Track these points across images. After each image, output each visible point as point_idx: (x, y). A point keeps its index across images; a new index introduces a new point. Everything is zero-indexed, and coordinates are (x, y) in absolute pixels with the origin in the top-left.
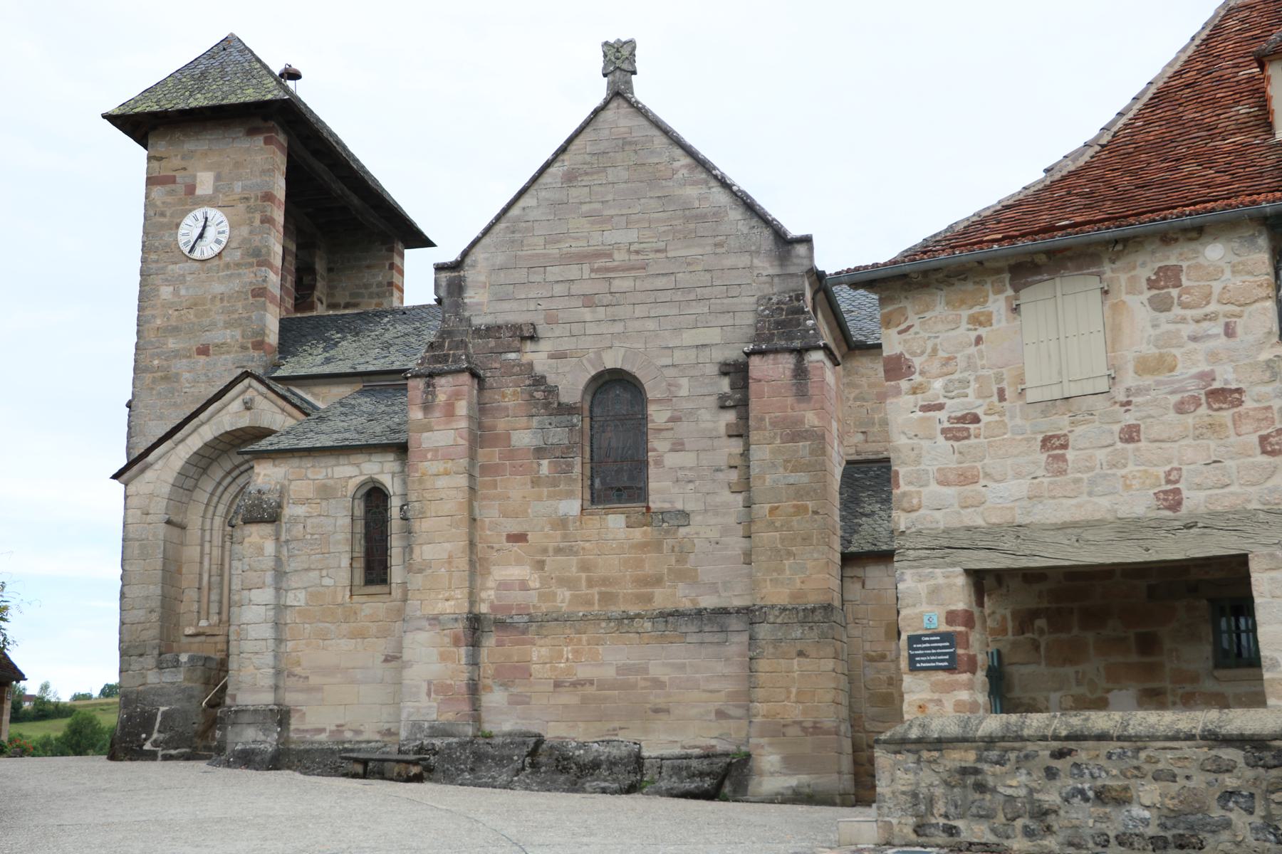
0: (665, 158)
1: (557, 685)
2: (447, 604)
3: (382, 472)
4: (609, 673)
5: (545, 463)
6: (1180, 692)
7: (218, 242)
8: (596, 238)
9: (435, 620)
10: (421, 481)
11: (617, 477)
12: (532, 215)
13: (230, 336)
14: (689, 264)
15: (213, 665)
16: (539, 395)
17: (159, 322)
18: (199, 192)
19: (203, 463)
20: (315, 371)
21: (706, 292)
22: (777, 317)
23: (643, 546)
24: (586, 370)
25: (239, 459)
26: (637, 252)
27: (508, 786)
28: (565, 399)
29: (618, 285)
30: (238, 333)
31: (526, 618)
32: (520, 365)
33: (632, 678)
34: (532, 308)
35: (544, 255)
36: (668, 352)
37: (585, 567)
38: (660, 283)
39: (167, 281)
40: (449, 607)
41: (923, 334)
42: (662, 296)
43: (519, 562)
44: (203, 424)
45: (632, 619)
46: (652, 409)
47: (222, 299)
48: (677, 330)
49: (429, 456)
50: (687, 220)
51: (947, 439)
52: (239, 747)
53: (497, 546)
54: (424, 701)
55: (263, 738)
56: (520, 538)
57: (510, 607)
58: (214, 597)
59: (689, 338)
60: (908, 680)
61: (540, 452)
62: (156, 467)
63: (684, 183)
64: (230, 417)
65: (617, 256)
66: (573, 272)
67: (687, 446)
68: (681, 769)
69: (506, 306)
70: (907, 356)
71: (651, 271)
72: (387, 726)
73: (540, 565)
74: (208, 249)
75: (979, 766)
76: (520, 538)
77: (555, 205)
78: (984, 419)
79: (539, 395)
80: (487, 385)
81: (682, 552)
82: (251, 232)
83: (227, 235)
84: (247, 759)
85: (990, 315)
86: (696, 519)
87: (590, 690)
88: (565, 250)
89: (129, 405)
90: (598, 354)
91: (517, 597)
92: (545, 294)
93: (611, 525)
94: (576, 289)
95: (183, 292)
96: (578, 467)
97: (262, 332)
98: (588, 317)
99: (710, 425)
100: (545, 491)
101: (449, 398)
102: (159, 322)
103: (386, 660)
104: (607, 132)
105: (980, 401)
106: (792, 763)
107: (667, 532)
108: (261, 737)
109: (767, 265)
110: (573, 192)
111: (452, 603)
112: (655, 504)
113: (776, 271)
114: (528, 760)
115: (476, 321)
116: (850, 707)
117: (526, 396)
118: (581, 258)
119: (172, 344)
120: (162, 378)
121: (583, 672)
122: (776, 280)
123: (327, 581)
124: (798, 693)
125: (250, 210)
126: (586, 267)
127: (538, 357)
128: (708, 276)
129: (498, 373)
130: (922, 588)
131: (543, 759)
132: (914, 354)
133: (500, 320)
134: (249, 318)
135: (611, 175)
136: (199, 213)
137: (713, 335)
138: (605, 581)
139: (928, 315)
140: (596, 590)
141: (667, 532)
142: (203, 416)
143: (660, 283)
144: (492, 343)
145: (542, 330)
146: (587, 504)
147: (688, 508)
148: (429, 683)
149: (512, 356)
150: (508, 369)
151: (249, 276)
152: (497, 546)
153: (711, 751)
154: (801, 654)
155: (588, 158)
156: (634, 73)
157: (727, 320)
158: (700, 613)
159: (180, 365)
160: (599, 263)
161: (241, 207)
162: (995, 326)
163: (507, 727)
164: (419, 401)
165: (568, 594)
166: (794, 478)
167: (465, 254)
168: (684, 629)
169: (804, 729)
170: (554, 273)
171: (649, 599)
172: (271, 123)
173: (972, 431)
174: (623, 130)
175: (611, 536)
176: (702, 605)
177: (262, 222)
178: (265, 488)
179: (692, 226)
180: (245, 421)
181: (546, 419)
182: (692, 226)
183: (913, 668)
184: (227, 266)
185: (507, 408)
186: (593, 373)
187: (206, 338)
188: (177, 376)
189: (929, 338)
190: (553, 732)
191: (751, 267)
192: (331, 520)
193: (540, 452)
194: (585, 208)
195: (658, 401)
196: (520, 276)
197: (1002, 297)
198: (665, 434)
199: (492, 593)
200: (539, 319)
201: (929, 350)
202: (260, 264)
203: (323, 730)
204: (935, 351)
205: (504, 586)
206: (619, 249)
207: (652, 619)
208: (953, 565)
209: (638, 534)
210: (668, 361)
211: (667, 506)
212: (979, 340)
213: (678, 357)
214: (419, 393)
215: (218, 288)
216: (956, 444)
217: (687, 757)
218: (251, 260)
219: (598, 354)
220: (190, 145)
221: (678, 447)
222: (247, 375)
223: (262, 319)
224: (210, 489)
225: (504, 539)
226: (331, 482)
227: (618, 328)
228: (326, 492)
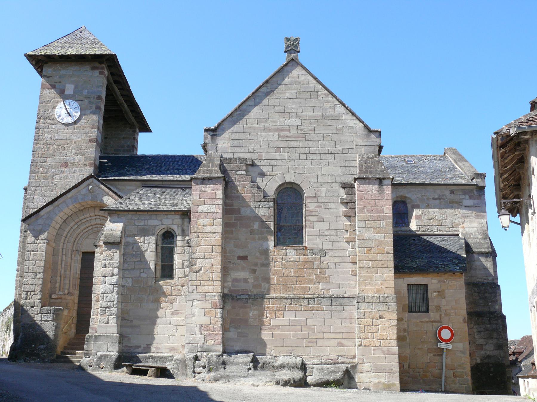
3: (173, 224)
8: (282, 122)
18: (67, 93)
24: (277, 182)
26: (301, 130)
30: (82, 158)
43: (243, 269)
53: (232, 262)
56: (244, 258)
58: (67, 282)
66: (271, 136)
69: (238, 149)
73: (254, 271)
76: (244, 258)
86: (329, 254)
89: (26, 189)
91: (242, 286)
92: (257, 145)
100: (257, 237)
112: (306, 243)
116: (122, 337)
118: (275, 131)
125: (90, 102)
148: (201, 326)
152: (232, 262)
156: (299, 52)
161: (86, 101)
167: (219, 125)
170: (263, 136)
172: (103, 65)
177: (96, 108)
183: (271, 324)
186: (280, 183)
194: (276, 108)
196: (246, 136)
198: (314, 213)
200: (254, 157)
205: (235, 280)
206: (293, 128)
220: (63, 72)
221: (321, 219)
224: (67, 230)
225: (236, 258)
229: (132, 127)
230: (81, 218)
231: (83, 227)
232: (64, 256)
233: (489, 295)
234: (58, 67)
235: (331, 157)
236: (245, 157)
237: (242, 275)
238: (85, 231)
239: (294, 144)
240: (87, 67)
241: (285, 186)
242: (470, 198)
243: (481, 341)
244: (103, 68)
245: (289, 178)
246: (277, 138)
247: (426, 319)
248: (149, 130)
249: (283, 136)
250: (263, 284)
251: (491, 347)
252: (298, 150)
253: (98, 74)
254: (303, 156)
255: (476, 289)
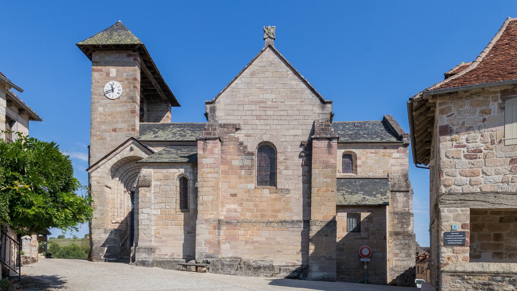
0: (284, 70)
1: (246, 243)
2: (211, 216)
4: (263, 239)
5: (243, 171)
6: (508, 254)
7: (118, 93)
8: (261, 96)
9: (207, 221)
10: (202, 175)
11: (268, 176)
12: (240, 86)
13: (124, 126)
14: (292, 107)
15: (122, 233)
16: (241, 148)
17: (98, 119)
18: (111, 75)
19: (117, 167)
20: (153, 139)
21: (297, 117)
22: (321, 127)
23: (275, 200)
25: (136, 165)
26: (275, 102)
27: (235, 274)
28: (249, 150)
29: (268, 113)
30: (126, 125)
31: (236, 221)
32: (235, 138)
33: (270, 241)
34: (239, 118)
35: (243, 101)
36: (285, 137)
37: (256, 206)
38: (282, 113)
39: (101, 106)
40: (212, 217)
41: (458, 117)
42: (283, 118)
43: (234, 203)
44: (117, 154)
45: (271, 223)
46: (278, 155)
47: (120, 113)
48: (288, 129)
49: (205, 166)
50: (292, 92)
51: (466, 158)
52: (140, 260)
54: (203, 247)
55: (148, 257)
56: (234, 195)
57: (231, 217)
59: (292, 132)
60: (443, 249)
61: (241, 167)
62: (101, 167)
63: (291, 79)
64: (125, 153)
65: (268, 103)
66: (253, 107)
67: (290, 168)
68: (287, 270)
69: (230, 117)
70: (450, 126)
71: (279, 109)
72: (189, 254)
73: (241, 204)
74: (114, 95)
75: (491, 282)
76: (234, 195)
77: (248, 83)
78: (484, 151)
79: (241, 148)
80: (224, 144)
81: (288, 202)
82: (130, 91)
83: (122, 91)
84: (143, 263)
85: (490, 110)
86: (292, 192)
87: (257, 244)
88: (250, 100)
90: (261, 136)
91: (233, 214)
93: (265, 192)
94: (254, 113)
95: (106, 110)
96: (255, 172)
97: (134, 125)
98: (258, 123)
99: (297, 162)
100: (243, 180)
101: (212, 147)
102: (98, 119)
103: (188, 233)
104: (266, 59)
105: (482, 145)
106: (321, 269)
107: (283, 195)
108: (147, 256)
109: (317, 110)
110: (253, 79)
111: (213, 215)
112: (279, 186)
113: (321, 112)
114: (239, 266)
115: (220, 122)
117: (237, 149)
118: (256, 103)
119: (103, 127)
120: (100, 139)
121: (255, 239)
122: (320, 115)
123: (167, 207)
124: (325, 247)
125: (129, 83)
126: (258, 106)
127: (240, 135)
128: (298, 112)
129: (228, 140)
130: (451, 215)
131: (242, 266)
132: (454, 125)
133: (228, 122)
134: (130, 120)
135: (267, 74)
136: (111, 82)
137: (299, 132)
138: (262, 210)
139: (461, 109)
140: (259, 213)
141: (283, 195)
142: (117, 151)
143: (282, 113)
144: (226, 130)
145: (242, 127)
146: (256, 186)
147: (289, 188)
148: (205, 241)
149: (232, 134)
150: (231, 139)
151: (129, 106)
153: (295, 264)
154: (326, 235)
155: (259, 68)
157: (304, 127)
158: (292, 222)
159: (107, 135)
160: (262, 105)
161: (126, 82)
162: (492, 114)
163: (230, 255)
164: (202, 148)
165: (250, 214)
166: (325, 180)
168: (287, 226)
169: (326, 259)
170: (247, 107)
171: (276, 216)
172: (136, 53)
173: (478, 156)
174: (271, 59)
175: (264, 196)
176: (294, 219)
177: (134, 87)
178: (146, 175)
179: (293, 95)
180: (132, 154)
181: (244, 157)
182: (293, 95)
184: (122, 102)
185: (230, 152)
187: (115, 126)
188: (105, 139)
189: (461, 119)
190: (245, 257)
191: (312, 110)
192: (169, 187)
193: (241, 167)
194: (257, 85)
195: (281, 153)
196: (235, 107)
197: (496, 104)
198: (282, 164)
199: (225, 213)
200: (241, 122)
201: (461, 123)
202: (133, 102)
203: (167, 255)
204: (463, 124)
205: (229, 211)
207: (277, 223)
208: (466, 206)
209: (273, 196)
210: (284, 140)
211: (283, 187)
212: (484, 120)
213: (288, 139)
214: (202, 145)
215: (119, 109)
216: (470, 161)
217: (288, 266)
218: (130, 100)
219: (261, 136)
221: (287, 168)
222: (132, 138)
223: (134, 121)
226: (169, 174)
227: (268, 127)
228: (167, 178)
229: (166, 102)
230: (128, 168)
231: (130, 174)
232: (119, 194)
233: (405, 220)
234: (103, 54)
235: (296, 123)
236: (235, 123)
237: (233, 206)
238: (132, 177)
239: (269, 113)
240: (124, 55)
241: (263, 144)
242: (398, 152)
243: (397, 251)
244: (136, 55)
245: (266, 138)
246: (257, 109)
247: (358, 237)
248: (178, 105)
249: (262, 107)
250: (247, 213)
251: (404, 255)
252: (272, 118)
253: (133, 60)
254: (275, 122)
255: (397, 216)
